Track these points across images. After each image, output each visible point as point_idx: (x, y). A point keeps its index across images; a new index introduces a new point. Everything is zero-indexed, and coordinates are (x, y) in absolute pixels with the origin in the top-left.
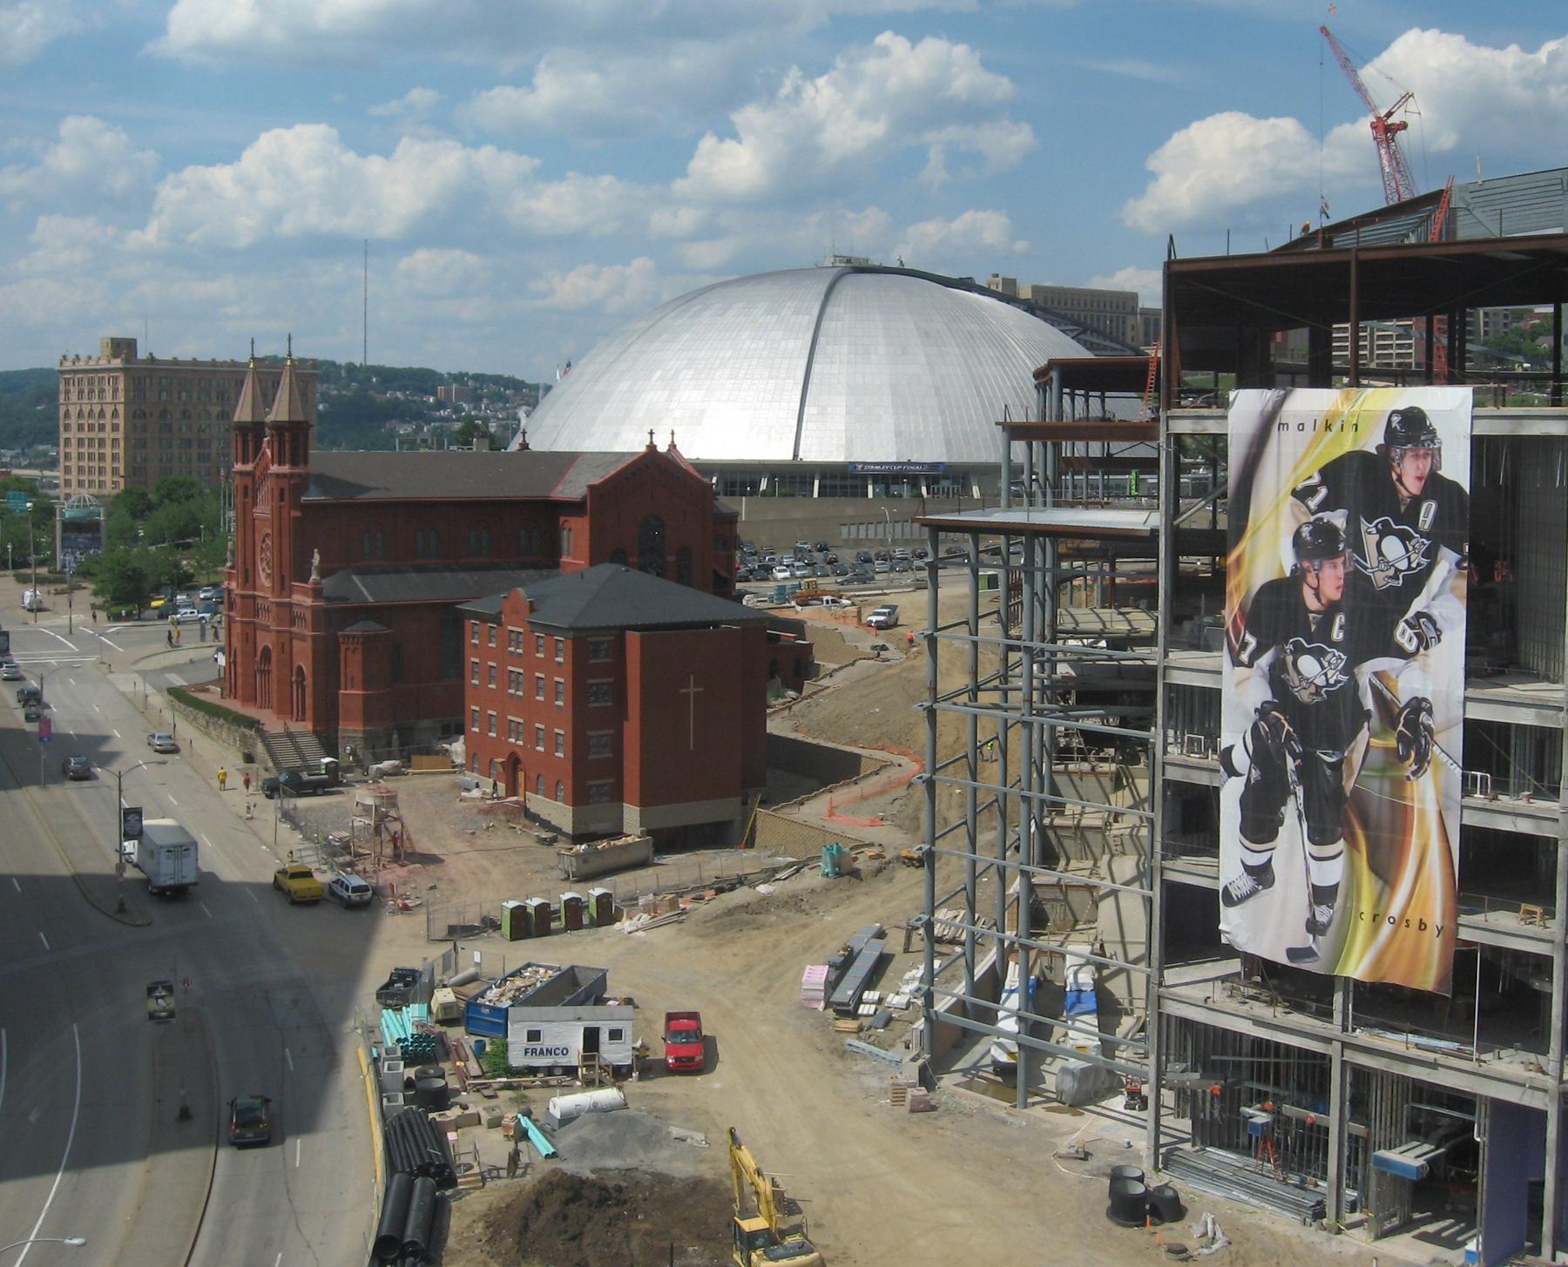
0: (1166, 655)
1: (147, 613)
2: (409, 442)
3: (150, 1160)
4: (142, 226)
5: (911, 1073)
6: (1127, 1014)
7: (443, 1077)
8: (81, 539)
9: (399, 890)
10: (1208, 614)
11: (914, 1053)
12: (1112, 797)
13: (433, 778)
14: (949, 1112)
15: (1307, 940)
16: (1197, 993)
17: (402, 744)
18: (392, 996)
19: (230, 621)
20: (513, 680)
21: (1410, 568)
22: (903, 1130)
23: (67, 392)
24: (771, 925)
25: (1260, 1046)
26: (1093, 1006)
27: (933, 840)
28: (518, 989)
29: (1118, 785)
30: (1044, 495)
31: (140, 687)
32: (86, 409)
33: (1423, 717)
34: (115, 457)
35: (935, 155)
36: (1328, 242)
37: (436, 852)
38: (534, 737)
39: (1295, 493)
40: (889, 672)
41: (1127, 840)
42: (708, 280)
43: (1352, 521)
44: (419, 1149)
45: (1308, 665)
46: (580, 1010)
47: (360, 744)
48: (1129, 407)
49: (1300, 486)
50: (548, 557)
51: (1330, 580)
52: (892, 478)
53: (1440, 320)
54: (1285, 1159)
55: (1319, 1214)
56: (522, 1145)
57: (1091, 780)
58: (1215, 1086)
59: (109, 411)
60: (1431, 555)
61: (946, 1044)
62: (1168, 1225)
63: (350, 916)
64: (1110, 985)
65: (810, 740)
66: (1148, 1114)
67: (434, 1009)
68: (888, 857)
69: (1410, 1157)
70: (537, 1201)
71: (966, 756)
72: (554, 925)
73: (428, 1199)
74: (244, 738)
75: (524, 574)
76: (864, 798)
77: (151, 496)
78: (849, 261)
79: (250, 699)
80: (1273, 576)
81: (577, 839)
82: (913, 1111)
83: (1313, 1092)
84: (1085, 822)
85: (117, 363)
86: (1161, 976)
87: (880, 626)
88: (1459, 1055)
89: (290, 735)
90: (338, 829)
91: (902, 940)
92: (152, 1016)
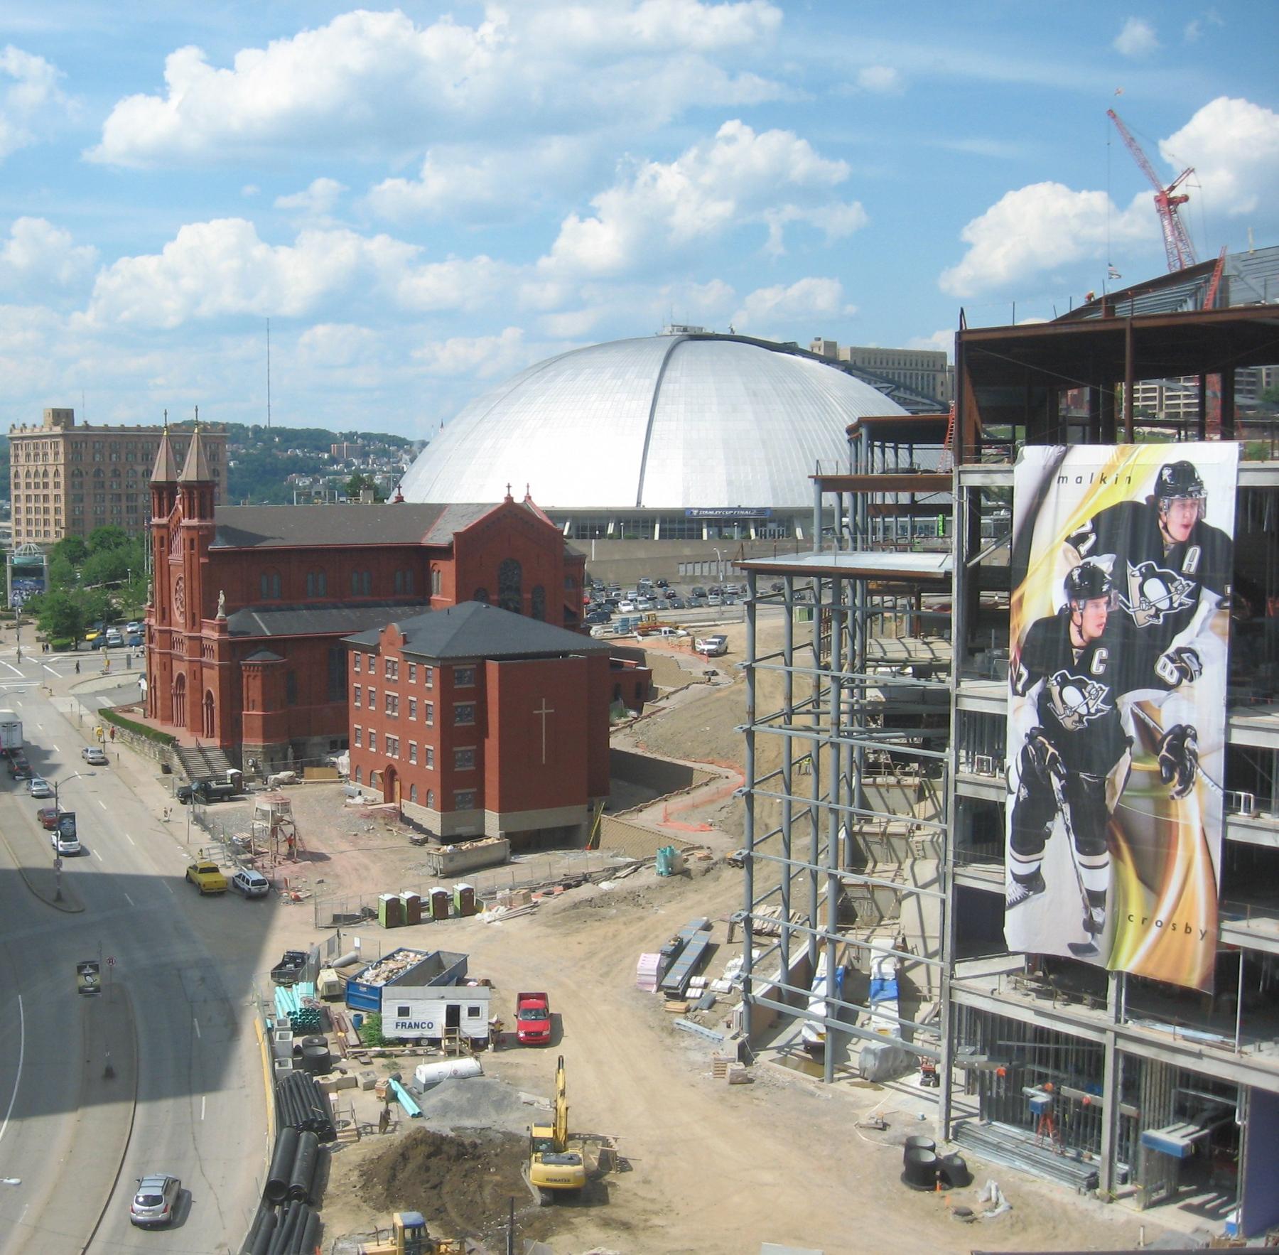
0: (958, 684)
1: (83, 645)
2: (307, 496)
3: (80, 1111)
4: (84, 310)
5: (732, 1049)
6: (925, 1000)
7: (326, 1045)
8: (29, 583)
9: (293, 884)
10: (997, 647)
11: (734, 1032)
12: (916, 807)
13: (324, 787)
14: (764, 1084)
15: (1088, 938)
16: (985, 985)
19: (151, 651)
20: (390, 702)
21: (1171, 607)
22: (722, 1100)
23: (17, 456)
24: (611, 918)
25: (1041, 1034)
26: (895, 994)
27: (752, 846)
28: (391, 971)
29: (921, 797)
30: (855, 540)
31: (76, 709)
32: (32, 470)
33: (1188, 743)
34: (57, 510)
35: (775, 231)
36: (1110, 311)
37: (324, 851)
39: (1068, 540)
40: (718, 695)
41: (928, 846)
42: (568, 347)
43: (1120, 568)
44: (304, 1106)
45: (1072, 695)
46: (443, 990)
48: (934, 458)
49: (1074, 534)
50: (420, 595)
51: (1092, 618)
52: (726, 522)
53: (1214, 380)
54: (1063, 1134)
55: (1093, 1184)
56: (392, 1106)
57: (897, 792)
58: (1000, 1068)
59: (51, 471)
60: (1195, 595)
61: (763, 1026)
62: (955, 1190)
63: (251, 906)
64: (910, 975)
65: (648, 755)
66: (941, 1091)
67: (320, 987)
68: (716, 858)
69: (1177, 1136)
70: (404, 1154)
71: (782, 772)
72: (423, 915)
73: (311, 1150)
74: (162, 752)
75: (399, 610)
76: (695, 806)
77: (86, 543)
78: (685, 330)
79: (168, 718)
80: (1045, 615)
81: (445, 840)
82: (732, 1083)
83: (1090, 1075)
84: (891, 829)
85: (58, 430)
86: (953, 969)
87: (712, 654)
88: (1221, 1046)
89: (201, 750)
90: (241, 831)
91: (727, 932)
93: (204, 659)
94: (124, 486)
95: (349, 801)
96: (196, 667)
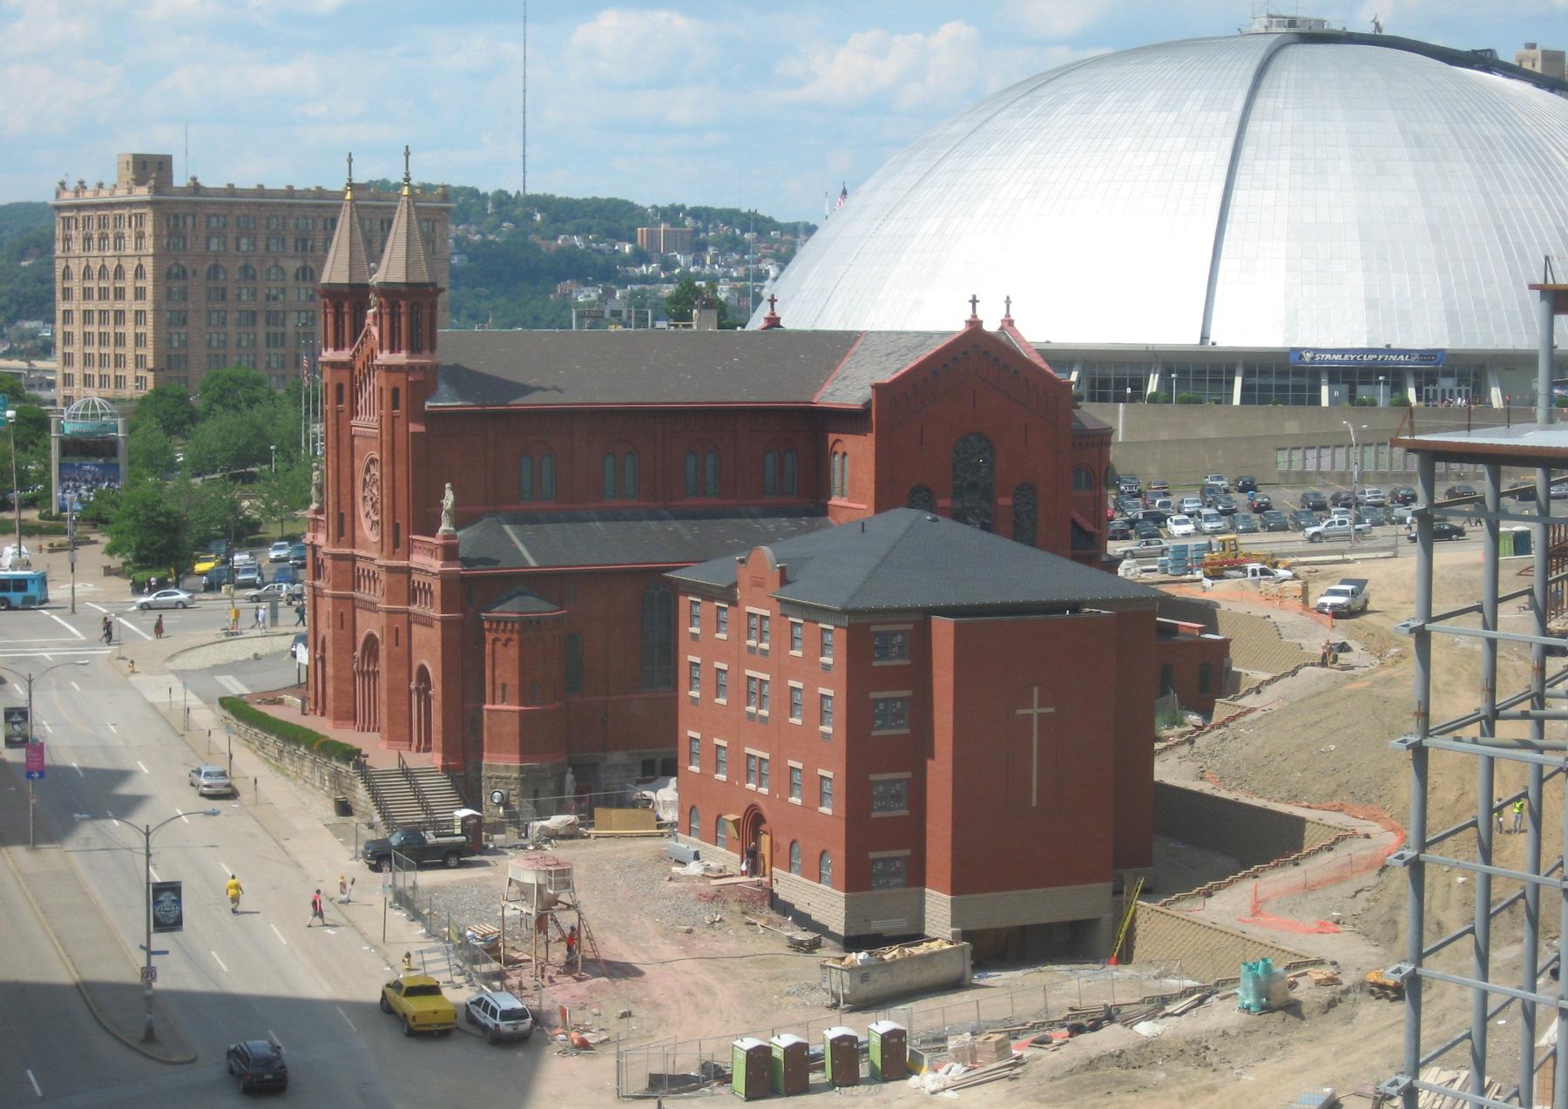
17: (579, 791)
20: (755, 692)
32: (96, 266)
47: (515, 789)
59: (130, 267)
74: (336, 776)
79: (347, 715)
85: (143, 193)
89: (407, 773)
93: (414, 608)
94: (261, 297)
95: (676, 869)
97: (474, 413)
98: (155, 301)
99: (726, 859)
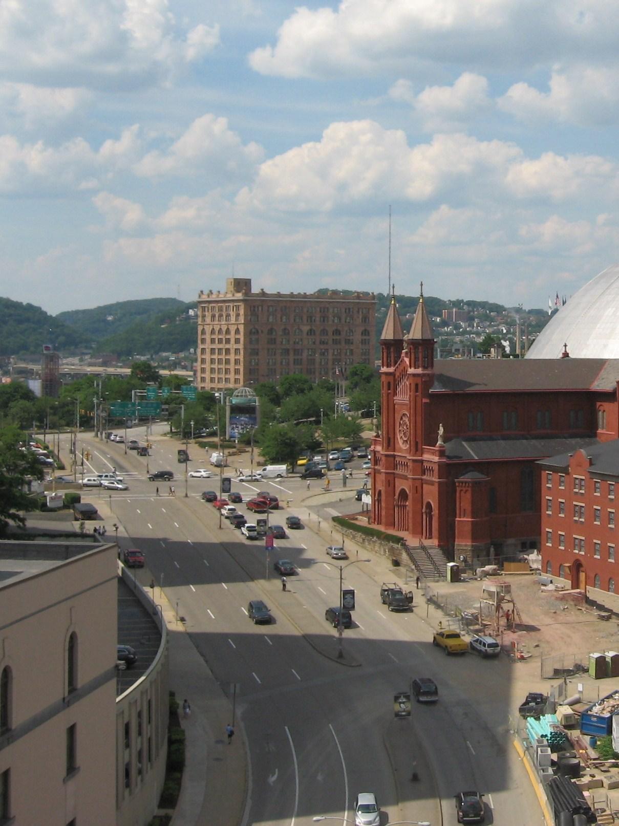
8: (244, 418)
17: (496, 555)
18: (530, 710)
20: (579, 511)
32: (217, 328)
38: (593, 548)
47: (470, 554)
50: (589, 430)
59: (233, 329)
74: (392, 550)
79: (392, 524)
85: (239, 296)
89: (423, 548)
92: (397, 715)
93: (424, 477)
94: (291, 342)
95: (543, 587)
96: (418, 483)
97: (448, 395)
98: (244, 345)
99: (564, 582)
